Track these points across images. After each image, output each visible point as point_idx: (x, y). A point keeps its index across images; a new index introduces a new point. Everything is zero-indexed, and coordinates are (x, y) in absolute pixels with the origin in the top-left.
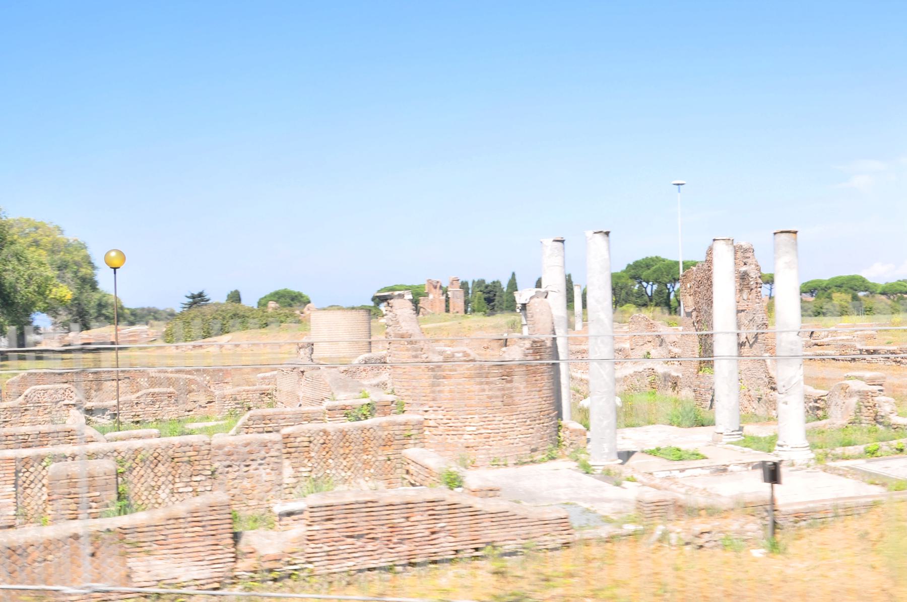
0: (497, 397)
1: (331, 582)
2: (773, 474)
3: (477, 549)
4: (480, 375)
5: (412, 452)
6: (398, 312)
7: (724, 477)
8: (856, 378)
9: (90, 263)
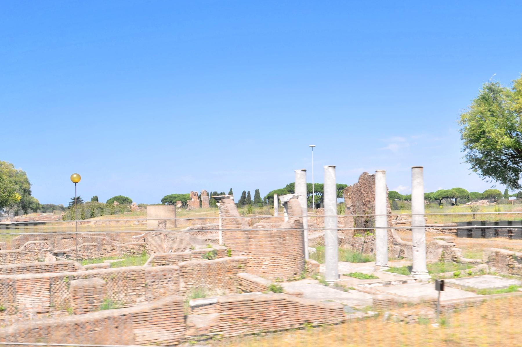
0: (278, 248)
1: (231, 341)
2: (441, 286)
3: (300, 324)
4: (271, 237)
5: (242, 275)
6: (228, 205)
7: (390, 287)
8: (440, 239)
9: (28, 182)
